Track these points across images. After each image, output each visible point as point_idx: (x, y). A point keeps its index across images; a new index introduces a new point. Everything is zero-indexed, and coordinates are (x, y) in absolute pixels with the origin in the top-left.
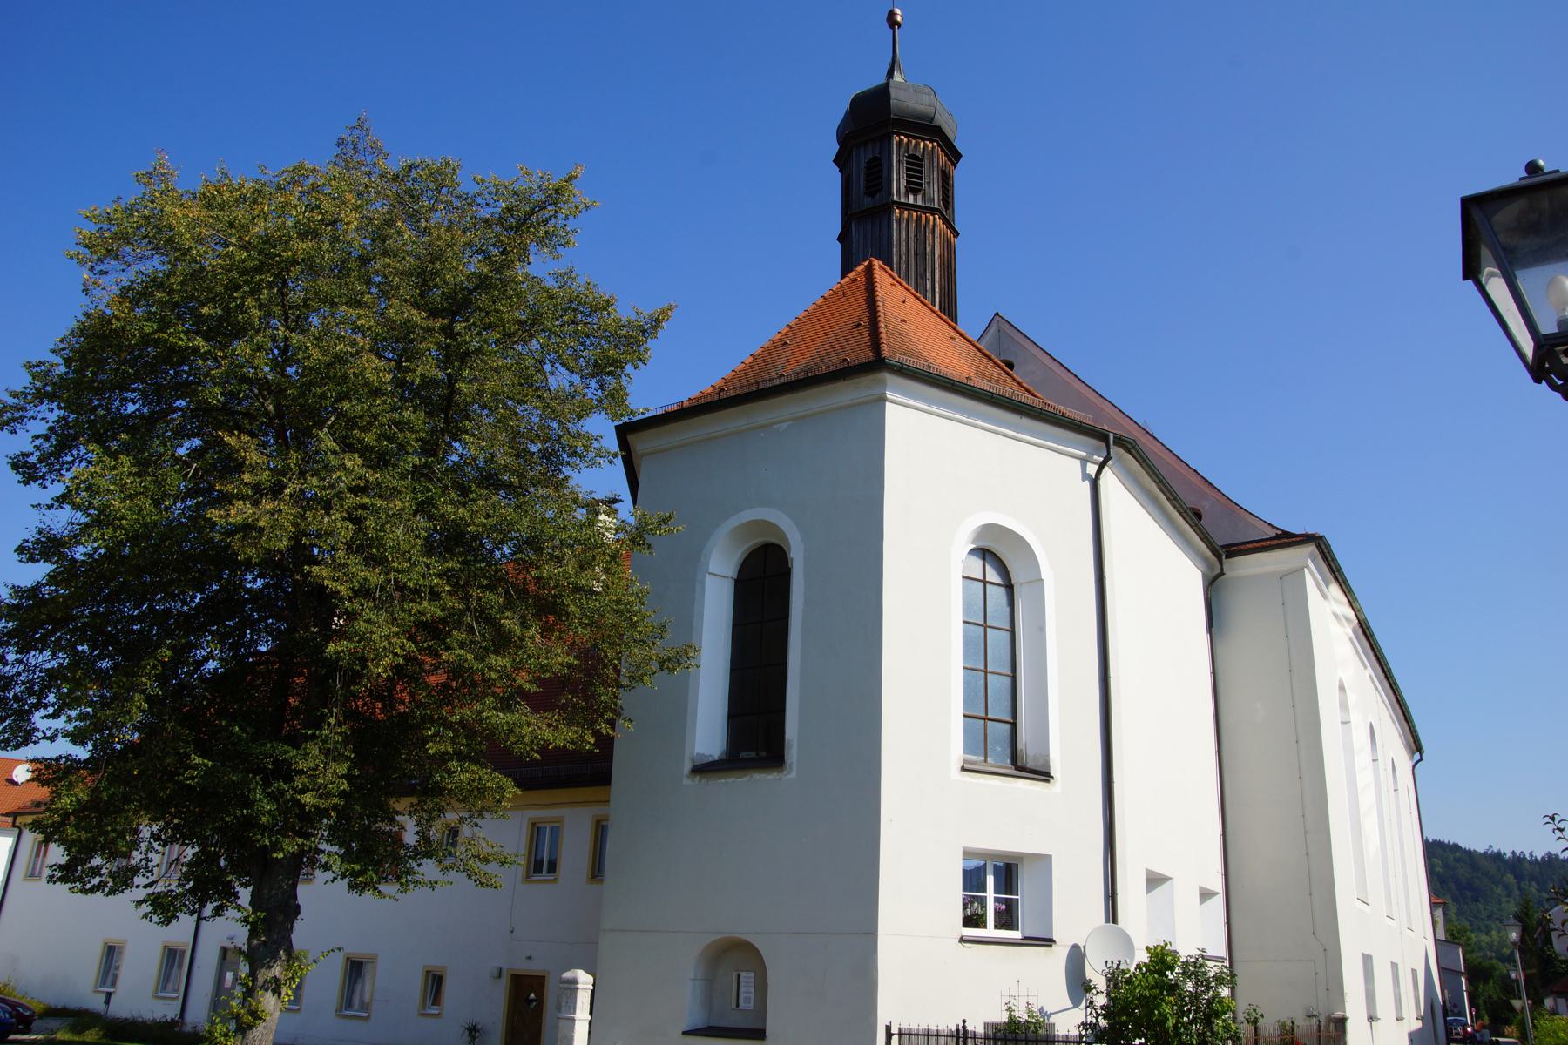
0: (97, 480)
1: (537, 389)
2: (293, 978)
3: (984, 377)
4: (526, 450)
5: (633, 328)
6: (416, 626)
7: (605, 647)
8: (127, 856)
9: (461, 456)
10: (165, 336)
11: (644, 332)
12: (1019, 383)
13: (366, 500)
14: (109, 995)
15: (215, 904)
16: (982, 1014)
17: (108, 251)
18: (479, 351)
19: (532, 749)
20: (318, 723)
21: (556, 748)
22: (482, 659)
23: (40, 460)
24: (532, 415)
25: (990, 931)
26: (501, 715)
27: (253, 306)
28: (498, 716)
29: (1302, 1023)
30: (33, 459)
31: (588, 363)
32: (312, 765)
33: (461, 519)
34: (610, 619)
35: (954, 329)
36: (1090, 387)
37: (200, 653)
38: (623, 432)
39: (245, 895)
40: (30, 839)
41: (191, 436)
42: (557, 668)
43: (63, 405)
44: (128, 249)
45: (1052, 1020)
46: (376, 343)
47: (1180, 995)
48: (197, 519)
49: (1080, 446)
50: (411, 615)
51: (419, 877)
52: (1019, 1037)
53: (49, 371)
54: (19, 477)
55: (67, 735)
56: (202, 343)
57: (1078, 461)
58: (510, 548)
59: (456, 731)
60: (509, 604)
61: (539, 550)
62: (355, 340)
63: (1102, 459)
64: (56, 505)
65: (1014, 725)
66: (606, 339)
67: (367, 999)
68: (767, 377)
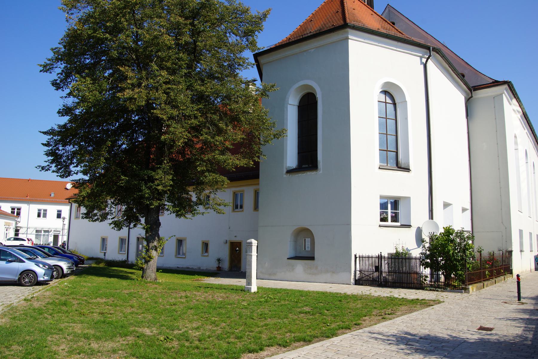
0: (80, 87)
1: (225, 43)
2: (161, 246)
3: (384, 28)
4: (223, 65)
5: (257, 18)
6: (190, 128)
7: (255, 131)
8: (105, 209)
9: (200, 69)
10: (96, 34)
11: (261, 19)
12: (397, 30)
13: (170, 86)
14: (105, 253)
15: (134, 223)
16: (387, 250)
17: (73, 6)
18: (204, 31)
19: (233, 168)
20: (161, 163)
21: (241, 167)
22: (213, 138)
23: (61, 82)
24: (224, 52)
25: (389, 223)
26: (221, 156)
27: (124, 21)
28: (220, 157)
29: (496, 252)
30: (58, 82)
31: (242, 32)
32: (160, 177)
33: (203, 90)
34: (256, 122)
35: (373, 11)
36: (423, 30)
37: (120, 143)
38: (256, 56)
39: (143, 220)
40: (75, 205)
41: (108, 69)
42: (239, 140)
43: (65, 62)
44: (79, 4)
45: (411, 252)
46: (168, 31)
47: (455, 243)
48: (114, 98)
49: (420, 52)
50: (188, 125)
51: (198, 211)
52: (399, 258)
53: (59, 50)
54: (55, 88)
55: (81, 172)
56: (108, 36)
57: (419, 58)
58: (220, 99)
59: (206, 163)
60: (221, 119)
61: (230, 99)
62: (160, 30)
63: (428, 56)
64: (68, 96)
65: (397, 153)
66: (248, 23)
67: (184, 252)
68: (305, 33)
